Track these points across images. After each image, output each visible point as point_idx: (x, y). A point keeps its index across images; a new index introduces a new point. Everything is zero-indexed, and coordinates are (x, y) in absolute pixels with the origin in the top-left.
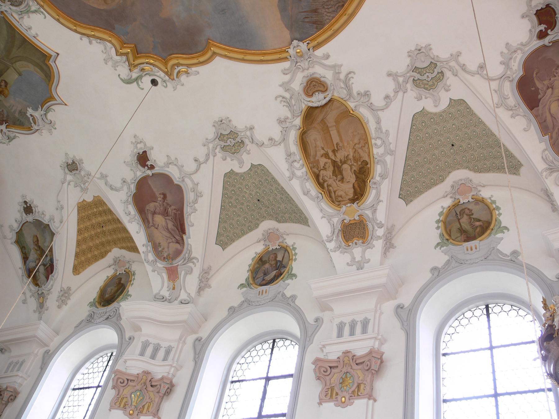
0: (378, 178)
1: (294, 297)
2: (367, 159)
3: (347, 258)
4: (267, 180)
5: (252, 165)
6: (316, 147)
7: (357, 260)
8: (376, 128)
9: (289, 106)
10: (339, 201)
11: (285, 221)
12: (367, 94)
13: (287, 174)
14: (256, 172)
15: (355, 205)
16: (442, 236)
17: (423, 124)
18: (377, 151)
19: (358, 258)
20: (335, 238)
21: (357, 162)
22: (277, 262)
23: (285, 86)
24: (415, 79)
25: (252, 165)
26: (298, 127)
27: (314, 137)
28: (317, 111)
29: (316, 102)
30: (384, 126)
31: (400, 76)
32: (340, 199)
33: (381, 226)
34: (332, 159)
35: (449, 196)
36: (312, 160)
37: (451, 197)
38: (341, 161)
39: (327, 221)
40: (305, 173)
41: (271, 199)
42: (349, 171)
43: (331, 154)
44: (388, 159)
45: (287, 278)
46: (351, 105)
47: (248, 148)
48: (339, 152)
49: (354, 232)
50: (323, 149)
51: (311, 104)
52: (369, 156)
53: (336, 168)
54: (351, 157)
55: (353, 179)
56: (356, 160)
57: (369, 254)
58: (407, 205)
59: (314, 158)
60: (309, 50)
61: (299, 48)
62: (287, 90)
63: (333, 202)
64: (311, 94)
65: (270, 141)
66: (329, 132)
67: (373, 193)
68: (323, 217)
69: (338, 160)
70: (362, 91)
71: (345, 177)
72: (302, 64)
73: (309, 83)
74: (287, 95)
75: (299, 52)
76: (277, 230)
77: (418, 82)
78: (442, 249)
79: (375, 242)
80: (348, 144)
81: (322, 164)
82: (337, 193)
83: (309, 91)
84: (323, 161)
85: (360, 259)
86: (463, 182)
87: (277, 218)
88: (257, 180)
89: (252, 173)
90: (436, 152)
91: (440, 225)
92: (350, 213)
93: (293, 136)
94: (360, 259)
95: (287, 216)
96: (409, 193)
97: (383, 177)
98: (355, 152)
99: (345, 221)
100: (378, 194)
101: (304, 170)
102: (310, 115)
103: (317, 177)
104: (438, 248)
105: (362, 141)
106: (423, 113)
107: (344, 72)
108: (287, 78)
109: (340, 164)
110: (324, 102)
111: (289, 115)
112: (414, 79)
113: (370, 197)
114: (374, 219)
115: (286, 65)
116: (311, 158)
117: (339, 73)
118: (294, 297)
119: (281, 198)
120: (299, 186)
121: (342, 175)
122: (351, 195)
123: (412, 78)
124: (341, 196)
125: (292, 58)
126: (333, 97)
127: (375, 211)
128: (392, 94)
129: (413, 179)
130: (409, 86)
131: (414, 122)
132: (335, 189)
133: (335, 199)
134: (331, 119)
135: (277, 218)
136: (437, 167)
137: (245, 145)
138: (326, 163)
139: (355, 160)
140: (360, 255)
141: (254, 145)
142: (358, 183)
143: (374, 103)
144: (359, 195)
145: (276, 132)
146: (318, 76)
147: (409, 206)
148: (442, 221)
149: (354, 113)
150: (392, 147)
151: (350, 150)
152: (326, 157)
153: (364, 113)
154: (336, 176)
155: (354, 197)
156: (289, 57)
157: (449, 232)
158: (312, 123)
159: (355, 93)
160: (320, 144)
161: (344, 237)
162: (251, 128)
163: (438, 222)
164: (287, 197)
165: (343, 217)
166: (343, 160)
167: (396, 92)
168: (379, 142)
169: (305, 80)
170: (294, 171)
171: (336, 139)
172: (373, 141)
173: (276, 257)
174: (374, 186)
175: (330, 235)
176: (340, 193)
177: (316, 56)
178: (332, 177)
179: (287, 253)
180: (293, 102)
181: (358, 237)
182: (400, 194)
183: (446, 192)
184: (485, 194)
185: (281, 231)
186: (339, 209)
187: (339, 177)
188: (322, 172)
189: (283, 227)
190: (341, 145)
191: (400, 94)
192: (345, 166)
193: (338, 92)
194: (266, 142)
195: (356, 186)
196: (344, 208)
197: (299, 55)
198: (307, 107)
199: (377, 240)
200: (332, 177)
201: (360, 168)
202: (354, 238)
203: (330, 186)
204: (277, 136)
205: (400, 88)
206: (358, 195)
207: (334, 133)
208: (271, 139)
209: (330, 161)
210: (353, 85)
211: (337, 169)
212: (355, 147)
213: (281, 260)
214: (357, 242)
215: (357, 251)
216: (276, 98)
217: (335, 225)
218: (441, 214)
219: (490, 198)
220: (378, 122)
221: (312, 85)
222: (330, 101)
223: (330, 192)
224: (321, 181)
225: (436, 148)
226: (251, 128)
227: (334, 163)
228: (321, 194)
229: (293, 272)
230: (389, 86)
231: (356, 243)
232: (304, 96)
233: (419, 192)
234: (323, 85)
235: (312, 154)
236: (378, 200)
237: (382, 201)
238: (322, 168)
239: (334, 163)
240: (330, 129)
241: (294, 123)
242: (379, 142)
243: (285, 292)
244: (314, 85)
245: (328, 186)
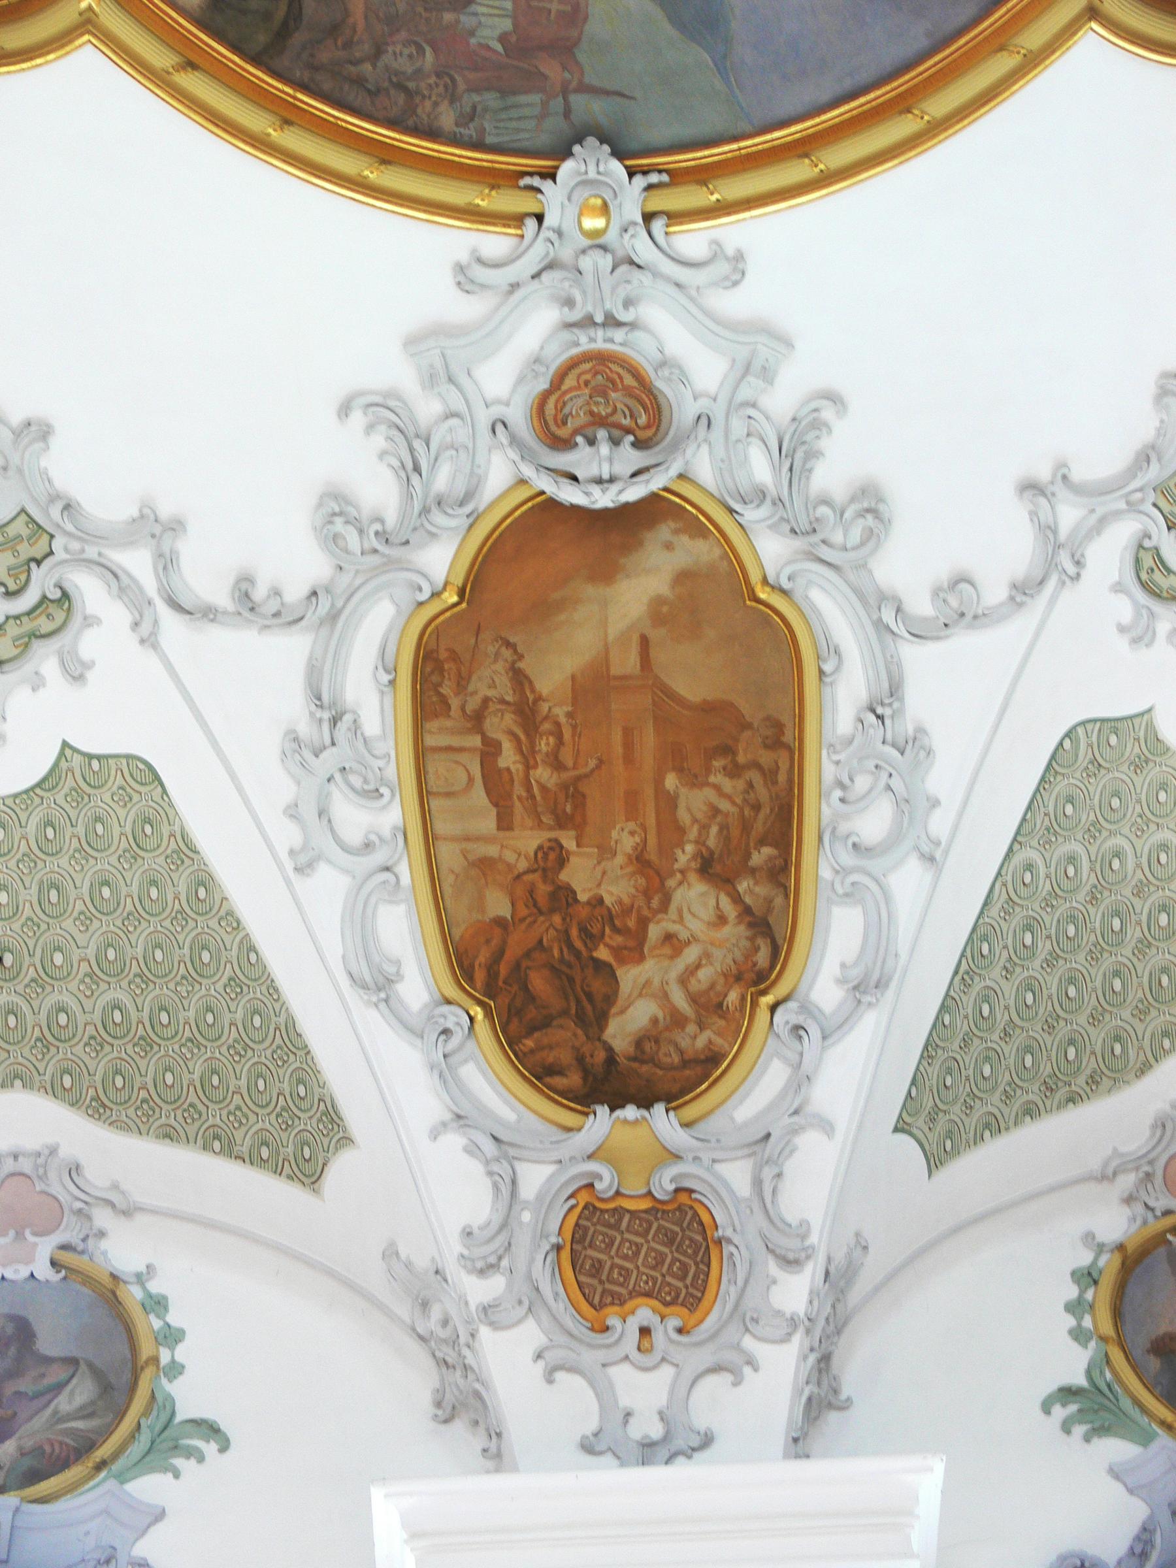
3: (574, 1404)
44: (907, 881)
45: (143, 1465)
68: (432, 1129)
86: (25, 1165)
145: (296, 562)
147: (942, 1175)
153: (828, 611)
184: (122, 1251)
216: (345, 410)
219: (140, 1279)
220: (466, 1061)
228: (773, 1008)
231: (645, 1331)
244: (599, 395)
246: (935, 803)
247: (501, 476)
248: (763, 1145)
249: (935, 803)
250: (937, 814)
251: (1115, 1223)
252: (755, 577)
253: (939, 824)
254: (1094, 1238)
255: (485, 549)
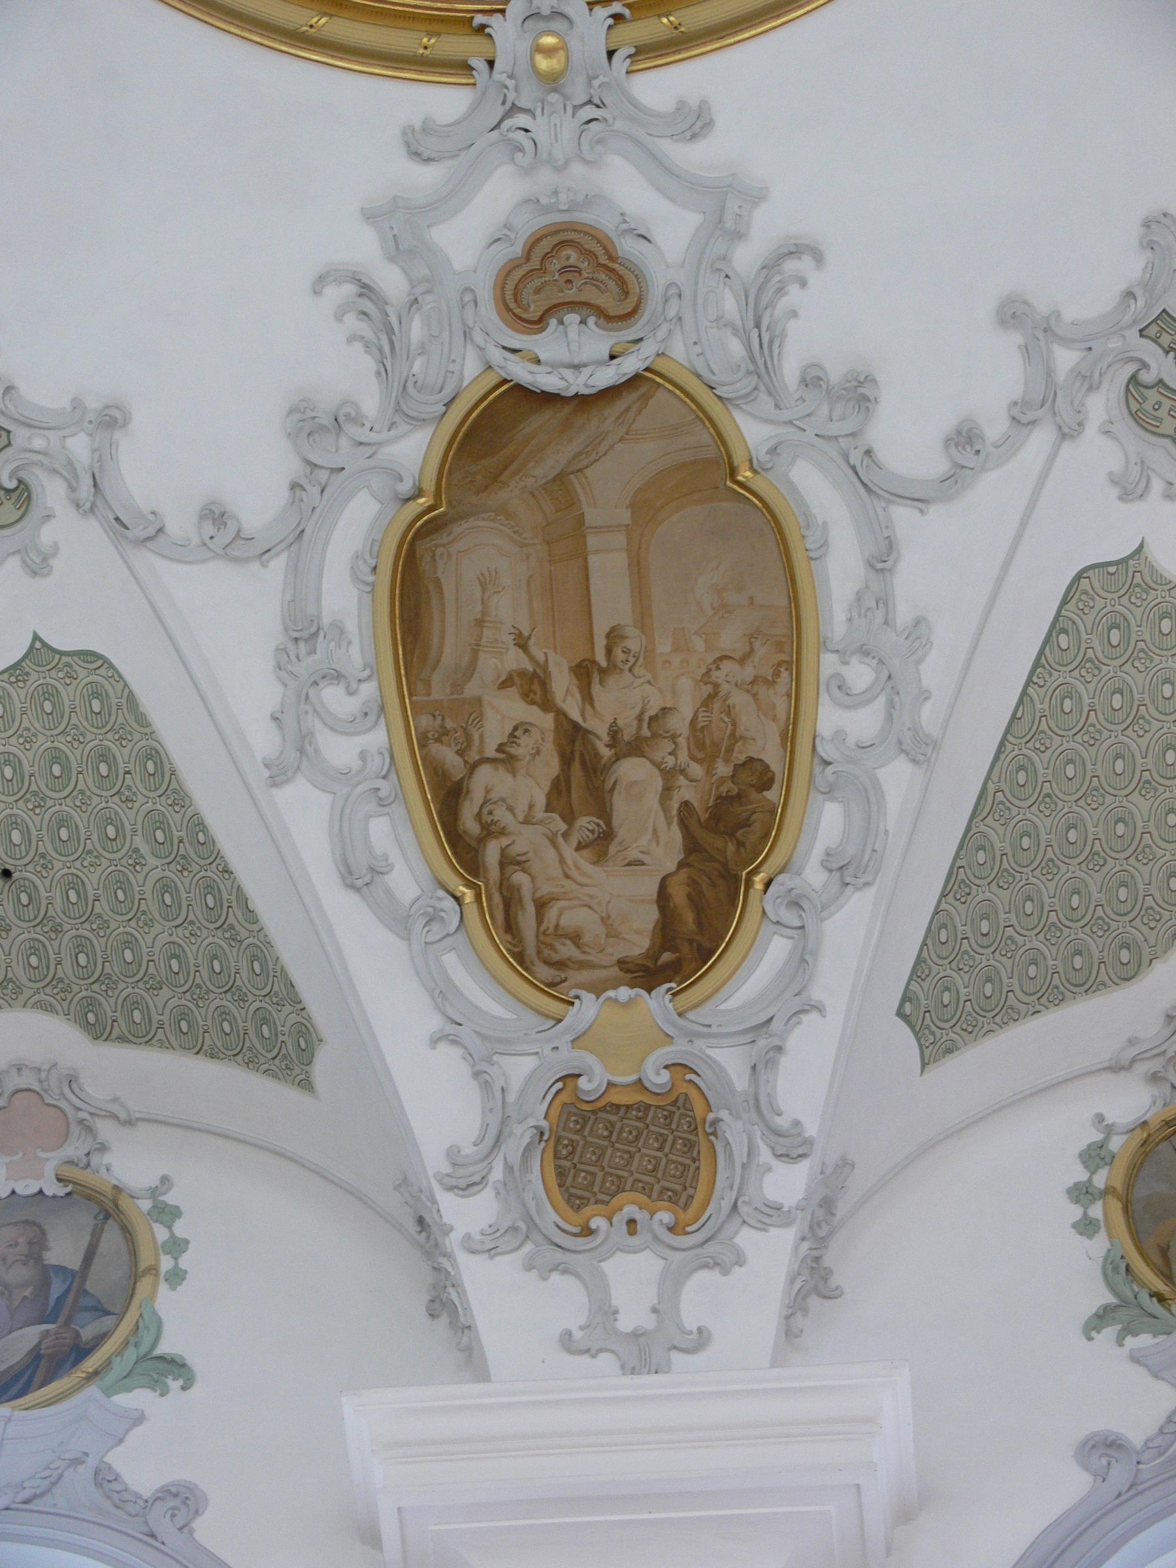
0: (813, 876)
1: (183, 1500)
2: (772, 756)
3: (564, 1302)
4: (104, 756)
5: (39, 649)
6: (480, 623)
7: (625, 1324)
8: (859, 597)
9: (386, 342)
10: (560, 965)
11: (141, 1035)
12: (859, 393)
13: (263, 740)
14: (49, 693)
15: (657, 1003)
16: (1116, 1270)
17: (1115, 636)
18: (833, 721)
19: (633, 1315)
20: (498, 1173)
21: (708, 761)
22: (46, 1274)
23: (402, 225)
24: (1147, 377)
25: (39, 649)
26: (406, 487)
27: (489, 566)
28: (542, 420)
29: (554, 366)
30: (912, 586)
31: (1064, 341)
32: (567, 950)
33: (791, 1146)
34: (561, 715)
35: (1142, 1068)
36: (439, 691)
37: (1155, 1078)
38: (615, 733)
39: (465, 1069)
40: (378, 763)
41: (93, 880)
42: (652, 800)
43: (562, 683)
44: (897, 778)
45: (126, 1382)
46: (752, 432)
47: (47, 534)
48: (611, 681)
49: (628, 1157)
50: (522, 643)
51: (521, 372)
52: (789, 738)
53: (576, 766)
54: (679, 723)
55: (664, 850)
56: (705, 747)
57: (700, 1300)
58: (924, 1065)
59: (457, 687)
60: (611, 54)
61: (558, 25)
62: (399, 250)
63: (520, 958)
64: (534, 313)
65: (209, 529)
66: (581, 555)
67: (775, 951)
68: (426, 1037)
69: (599, 727)
70: (835, 373)
71: (623, 831)
72: (540, 127)
73: (545, 246)
74: (392, 282)
75: (549, 52)
76: (72, 1081)
77: (1153, 396)
78: (1130, 1341)
79: (746, 1238)
80: (676, 649)
81: (493, 732)
82: (552, 914)
83: (527, 294)
84: (504, 712)
85: (648, 1322)
87: (91, 1004)
88: (42, 743)
89: (18, 696)
90: (1140, 806)
91: (1096, 1211)
92: (621, 1038)
93: (360, 525)
94: (648, 1322)
95: (164, 1002)
96: (948, 1004)
97: (847, 872)
98: (707, 702)
99: (583, 1083)
100: (803, 961)
101: (377, 738)
102: (498, 429)
103: (448, 797)
104: (1109, 1333)
105: (761, 650)
106: (1129, 574)
107: (767, 228)
108: (427, 178)
109: (606, 752)
110: (607, 377)
111: (371, 402)
112: (1133, 379)
113: (755, 969)
114: (759, 1105)
115: (445, 102)
116: (436, 678)
117: (739, 235)
118: (183, 1500)
119: (165, 886)
120: (318, 839)
121: (604, 811)
122: (638, 940)
123: (1130, 369)
124: (576, 938)
125: (497, 75)
126: (661, 365)
127: (763, 1065)
128: (995, 429)
129: (985, 927)
130: (1101, 405)
131: (1070, 610)
132: (545, 890)
133: (535, 949)
134: (608, 491)
135: (91, 1004)
136: (1123, 894)
137: (36, 513)
138: (519, 730)
139: (701, 745)
140: (652, 1298)
141: (93, 531)
142: (693, 883)
143: (881, 454)
144: (686, 950)
146: (606, 222)
147: (937, 1072)
148: (1108, 1191)
149: (758, 484)
150: (929, 716)
151: (686, 683)
152: (526, 696)
153: (814, 491)
154: (569, 818)
155: (653, 954)
156: (479, 64)
157: (1156, 1258)
158: (495, 479)
159: (790, 370)
160: (509, 610)
161: (561, 1174)
162: (111, 421)
163: (1081, 1193)
164: (210, 888)
165: (568, 1058)
166: (627, 735)
167: (1021, 419)
168: (860, 675)
169: (528, 225)
170: (311, 734)
171: (612, 604)
172: (829, 663)
173: (38, 1243)
174: (790, 917)
175: (468, 1150)
176: (572, 917)
177: (635, 104)
178: (539, 814)
179: (112, 1237)
180: (417, 330)
181: (646, 1190)
182: (906, 998)
183: (1132, 1042)
185: (95, 1090)
186: (555, 1007)
187: (586, 823)
188: (484, 775)
189: (114, 1071)
190: (633, 644)
191: (1040, 440)
192: (633, 770)
193: (690, 340)
194: (180, 524)
195: (679, 894)
196: (588, 1008)
197: (543, 63)
198: (491, 380)
199: (763, 1227)
200: (539, 814)
201: (724, 801)
202: (620, 1190)
203: (520, 863)
204: (259, 503)
205: (1043, 407)
206: (685, 945)
207: (608, 568)
208: (216, 515)
209: (547, 721)
210: (792, 326)
211: (583, 775)
212: (718, 676)
213: (75, 1264)
214: (640, 1216)
215: (632, 1274)
216: (320, 283)
217: (511, 1098)
218: (1094, 1156)
220: (882, 559)
221: (555, 265)
222: (635, 380)
223: (510, 900)
224: (469, 823)
225: (1145, 785)
226: (111, 421)
227: (572, 736)
228: (458, 899)
229: (164, 1348)
230: (994, 377)
231: (632, 1222)
232: (488, 310)
233: (995, 1012)
234: (622, 282)
235: (447, 659)
236: (797, 996)
237: (819, 1008)
238: (491, 752)
239: (572, 736)
240: (592, 541)
241: (386, 453)
242: (860, 675)
243: (117, 1459)
244: (570, 269)
245: (506, 861)
246: (925, 696)
247: (475, 357)
248: (764, 1037)
249: (925, 696)
250: (927, 709)
251: (1131, 1103)
252: (739, 458)
253: (929, 716)
254: (1103, 1120)
255: (492, 397)
